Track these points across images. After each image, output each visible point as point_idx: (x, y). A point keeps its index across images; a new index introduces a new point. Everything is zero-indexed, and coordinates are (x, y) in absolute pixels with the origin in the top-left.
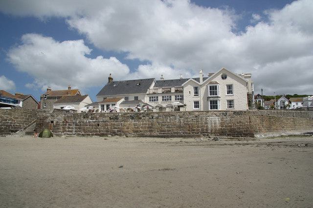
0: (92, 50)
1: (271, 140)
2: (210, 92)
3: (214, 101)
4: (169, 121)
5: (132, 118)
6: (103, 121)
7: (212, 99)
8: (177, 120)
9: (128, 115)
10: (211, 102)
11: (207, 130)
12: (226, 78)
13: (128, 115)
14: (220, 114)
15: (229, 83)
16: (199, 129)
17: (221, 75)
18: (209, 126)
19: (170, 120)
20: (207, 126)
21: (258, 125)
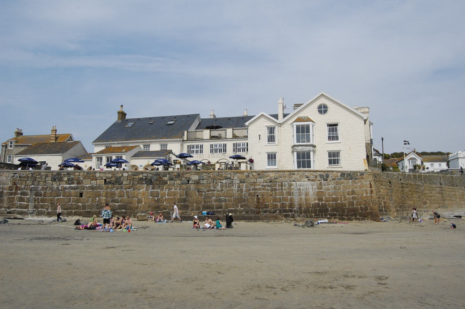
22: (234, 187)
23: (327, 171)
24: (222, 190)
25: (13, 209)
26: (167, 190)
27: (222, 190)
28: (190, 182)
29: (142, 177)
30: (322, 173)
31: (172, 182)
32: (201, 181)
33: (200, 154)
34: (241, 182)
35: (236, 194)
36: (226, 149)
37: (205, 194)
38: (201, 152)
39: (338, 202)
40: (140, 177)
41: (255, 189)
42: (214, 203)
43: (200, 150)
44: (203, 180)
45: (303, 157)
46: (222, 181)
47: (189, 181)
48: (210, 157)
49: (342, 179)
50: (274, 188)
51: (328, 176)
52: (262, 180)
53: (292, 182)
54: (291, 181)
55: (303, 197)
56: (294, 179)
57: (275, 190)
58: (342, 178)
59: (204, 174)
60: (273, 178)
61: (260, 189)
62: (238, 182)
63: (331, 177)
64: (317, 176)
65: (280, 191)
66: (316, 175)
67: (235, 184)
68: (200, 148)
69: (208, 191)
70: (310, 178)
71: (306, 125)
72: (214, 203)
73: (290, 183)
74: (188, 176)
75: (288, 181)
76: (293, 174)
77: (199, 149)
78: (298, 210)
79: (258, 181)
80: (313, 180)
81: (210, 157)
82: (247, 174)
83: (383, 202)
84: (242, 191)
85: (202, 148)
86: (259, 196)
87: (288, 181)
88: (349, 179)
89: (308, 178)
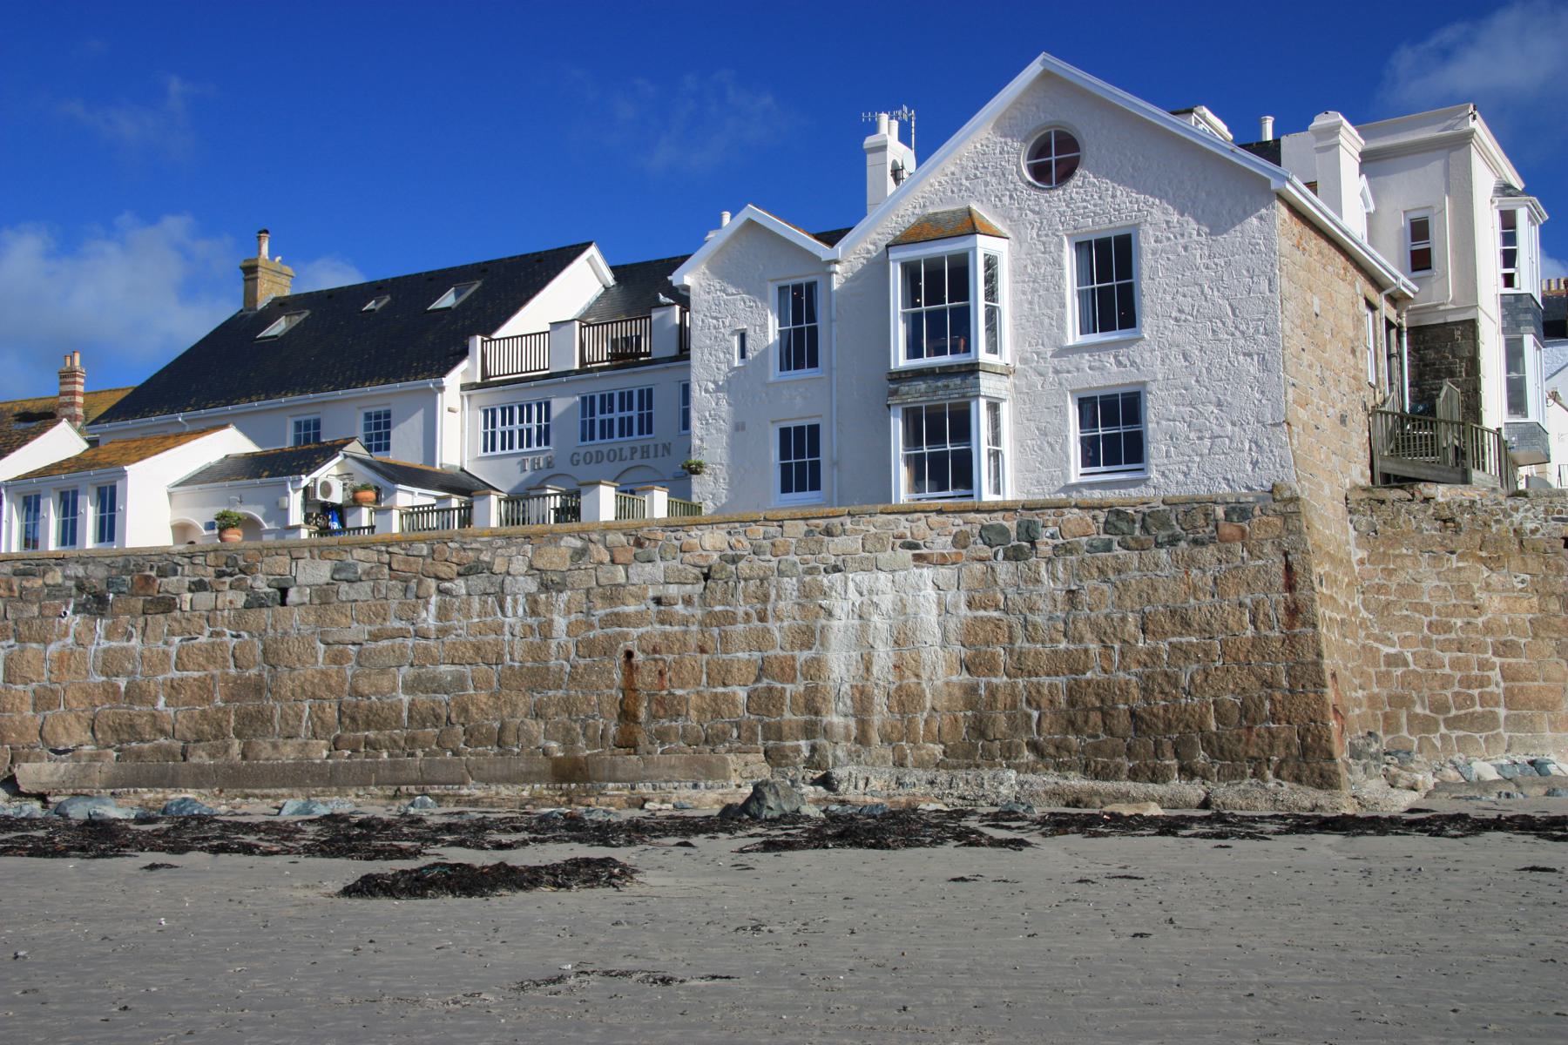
0: (670, 278)
1: (454, 820)
2: (914, 322)
3: (935, 417)
4: (429, 619)
5: (95, 603)
6: (9, 647)
7: (918, 393)
8: (515, 616)
9: (55, 577)
10: (912, 418)
11: (812, 704)
12: (1066, 173)
13: (55, 577)
14: (960, 541)
15: (1100, 226)
16: (731, 700)
17: (1529, 340)
18: (839, 665)
19: (443, 613)
20: (815, 668)
21: (1505, 648)
22: (510, 612)
23: (1028, 507)
24: (444, 632)
25: (261, 950)
26: (177, 639)
27: (444, 632)
28: (293, 595)
29: (60, 580)
30: (998, 519)
31: (205, 599)
32: (344, 587)
33: (603, 441)
34: (545, 587)
35: (517, 653)
36: (650, 416)
37: (359, 654)
38: (646, 425)
39: (1089, 675)
40: (49, 581)
41: (618, 620)
42: (402, 696)
43: (641, 417)
44: (356, 586)
45: (936, 437)
46: (447, 585)
47: (284, 592)
48: (581, 462)
49: (1115, 546)
50: (718, 608)
51: (1029, 533)
52: (657, 570)
53: (819, 578)
54: (811, 571)
55: (884, 657)
56: (832, 560)
57: (730, 618)
58: (1116, 539)
59: (355, 556)
60: (716, 556)
61: (640, 619)
62: (532, 586)
63: (1052, 536)
64: (966, 535)
65: (756, 623)
66: (963, 528)
67: (516, 594)
68: (641, 408)
69: (375, 637)
70: (924, 551)
71: (952, 258)
72: (402, 696)
73: (808, 578)
74: (281, 564)
75: (800, 567)
76: (828, 532)
77: (635, 413)
78: (847, 727)
79: (635, 580)
80: (943, 561)
81: (581, 462)
82: (578, 544)
83: (1495, 675)
84: (546, 631)
85: (650, 407)
86: (639, 657)
87: (800, 567)
88: (1159, 545)
89: (917, 547)
